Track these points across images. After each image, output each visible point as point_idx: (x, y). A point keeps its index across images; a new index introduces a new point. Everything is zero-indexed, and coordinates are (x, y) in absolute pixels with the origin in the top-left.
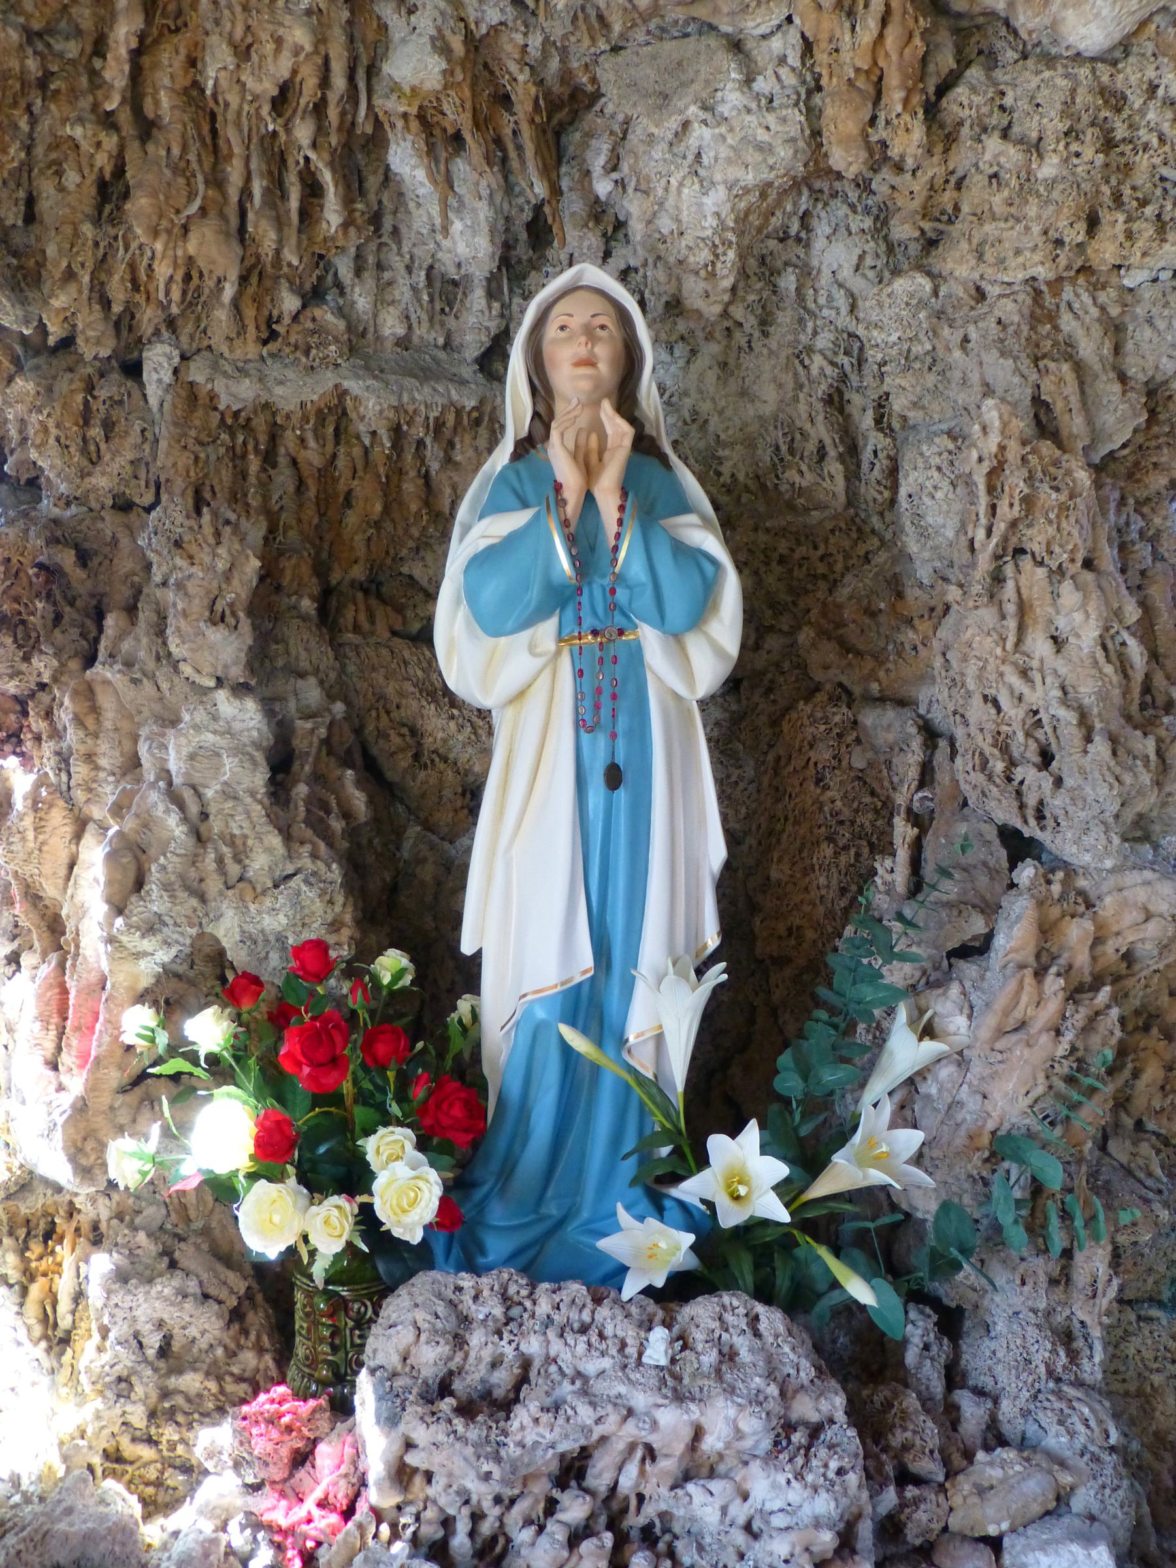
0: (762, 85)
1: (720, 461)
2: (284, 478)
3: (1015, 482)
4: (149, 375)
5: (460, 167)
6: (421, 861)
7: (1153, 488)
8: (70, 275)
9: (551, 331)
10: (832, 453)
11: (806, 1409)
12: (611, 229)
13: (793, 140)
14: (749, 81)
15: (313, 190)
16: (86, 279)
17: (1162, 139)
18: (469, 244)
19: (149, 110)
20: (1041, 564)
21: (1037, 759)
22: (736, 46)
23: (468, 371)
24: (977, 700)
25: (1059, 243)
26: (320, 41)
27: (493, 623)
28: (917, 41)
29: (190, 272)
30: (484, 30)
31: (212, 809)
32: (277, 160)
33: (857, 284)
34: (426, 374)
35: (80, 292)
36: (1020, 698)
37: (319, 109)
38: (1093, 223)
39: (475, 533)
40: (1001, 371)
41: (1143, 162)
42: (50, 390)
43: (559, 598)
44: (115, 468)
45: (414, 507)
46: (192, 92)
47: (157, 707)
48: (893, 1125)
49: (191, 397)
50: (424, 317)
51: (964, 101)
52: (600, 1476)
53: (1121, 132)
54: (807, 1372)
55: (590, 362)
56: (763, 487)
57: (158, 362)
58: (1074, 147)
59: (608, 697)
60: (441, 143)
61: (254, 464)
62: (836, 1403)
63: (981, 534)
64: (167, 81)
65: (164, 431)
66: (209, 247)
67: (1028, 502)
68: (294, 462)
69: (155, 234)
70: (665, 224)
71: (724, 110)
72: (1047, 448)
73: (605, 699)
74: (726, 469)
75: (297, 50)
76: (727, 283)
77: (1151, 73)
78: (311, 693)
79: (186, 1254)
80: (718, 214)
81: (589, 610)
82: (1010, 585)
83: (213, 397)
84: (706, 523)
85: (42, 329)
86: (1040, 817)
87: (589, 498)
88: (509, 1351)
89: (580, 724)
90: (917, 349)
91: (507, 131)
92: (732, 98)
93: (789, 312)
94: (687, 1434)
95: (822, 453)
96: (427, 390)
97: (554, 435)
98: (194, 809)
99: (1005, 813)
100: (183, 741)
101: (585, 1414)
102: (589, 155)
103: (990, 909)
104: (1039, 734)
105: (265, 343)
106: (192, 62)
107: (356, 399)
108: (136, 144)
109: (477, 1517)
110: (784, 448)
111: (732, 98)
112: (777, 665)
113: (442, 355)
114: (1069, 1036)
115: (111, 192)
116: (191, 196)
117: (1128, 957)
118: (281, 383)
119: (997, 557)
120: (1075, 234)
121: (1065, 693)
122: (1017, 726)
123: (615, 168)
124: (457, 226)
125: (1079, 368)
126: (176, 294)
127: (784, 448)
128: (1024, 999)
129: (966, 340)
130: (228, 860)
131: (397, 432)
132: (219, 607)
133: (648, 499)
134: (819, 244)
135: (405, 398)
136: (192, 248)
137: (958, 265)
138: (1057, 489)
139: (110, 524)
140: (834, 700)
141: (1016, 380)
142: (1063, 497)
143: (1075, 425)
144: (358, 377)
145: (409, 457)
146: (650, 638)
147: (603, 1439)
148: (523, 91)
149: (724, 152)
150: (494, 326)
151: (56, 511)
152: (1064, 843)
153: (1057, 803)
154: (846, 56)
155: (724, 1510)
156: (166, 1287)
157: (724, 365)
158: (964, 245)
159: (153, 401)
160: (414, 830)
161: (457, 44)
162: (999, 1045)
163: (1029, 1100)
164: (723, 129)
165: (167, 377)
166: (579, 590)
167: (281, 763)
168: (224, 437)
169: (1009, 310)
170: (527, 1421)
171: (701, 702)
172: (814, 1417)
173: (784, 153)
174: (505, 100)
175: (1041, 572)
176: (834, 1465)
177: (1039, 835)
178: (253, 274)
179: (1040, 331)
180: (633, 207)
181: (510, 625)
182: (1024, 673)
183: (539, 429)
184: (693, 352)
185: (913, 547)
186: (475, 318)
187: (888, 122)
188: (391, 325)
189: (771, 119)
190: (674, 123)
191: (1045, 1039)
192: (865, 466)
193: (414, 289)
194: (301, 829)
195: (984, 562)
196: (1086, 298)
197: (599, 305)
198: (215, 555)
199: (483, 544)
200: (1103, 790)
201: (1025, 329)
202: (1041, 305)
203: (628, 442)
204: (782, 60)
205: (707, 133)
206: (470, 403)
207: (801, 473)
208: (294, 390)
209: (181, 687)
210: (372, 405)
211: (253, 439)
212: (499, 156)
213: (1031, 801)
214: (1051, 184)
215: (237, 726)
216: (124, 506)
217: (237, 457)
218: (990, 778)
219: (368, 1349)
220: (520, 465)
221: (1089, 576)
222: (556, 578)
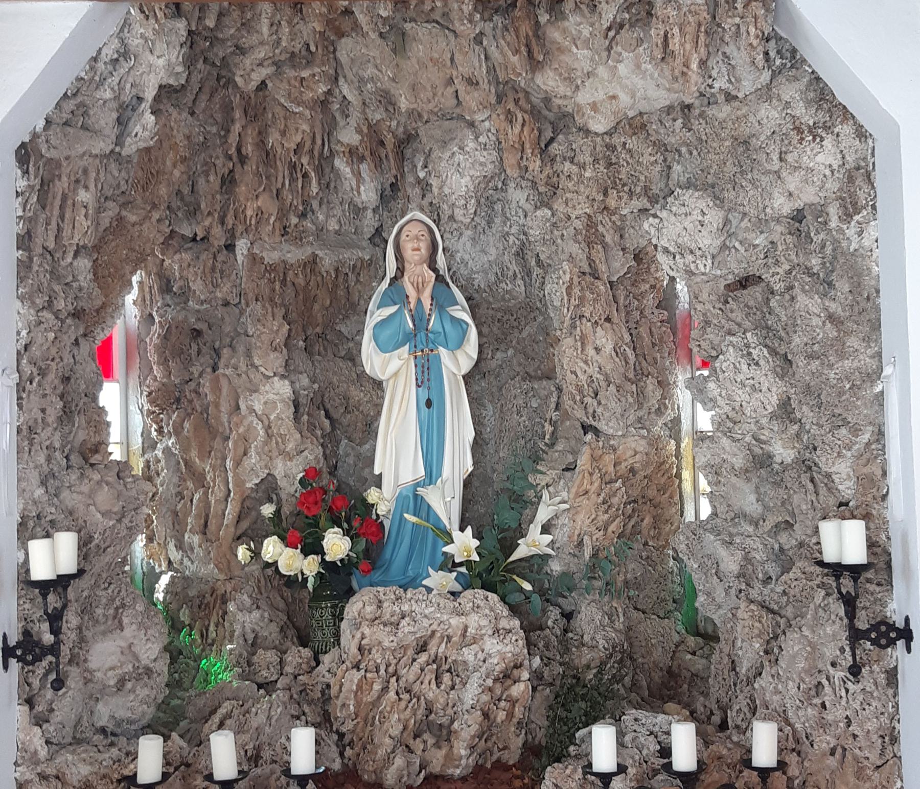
0: (482, 139)
1: (474, 279)
2: (290, 291)
3: (576, 291)
4: (238, 252)
5: (364, 167)
6: (348, 455)
7: (643, 289)
8: (209, 213)
9: (403, 237)
10: (519, 276)
11: (504, 624)
12: (425, 187)
13: (494, 162)
14: (477, 138)
15: (305, 176)
16: (216, 216)
17: (627, 162)
18: (368, 194)
19: (244, 152)
20: (590, 321)
21: (593, 395)
22: (472, 124)
23: (365, 243)
24: (568, 373)
25: (594, 200)
26: (312, 127)
27: (383, 347)
28: (535, 131)
29: (260, 212)
30: (375, 121)
31: (273, 425)
32: (293, 167)
33: (528, 207)
34: (349, 246)
35: (213, 220)
36: (585, 372)
37: (311, 151)
38: (606, 194)
39: (376, 315)
40: (574, 248)
41: (624, 170)
42: (198, 258)
43: (409, 338)
44: (225, 289)
45: (343, 302)
46: (261, 143)
47: (248, 385)
48: (541, 533)
49: (254, 259)
50: (347, 222)
51: (555, 148)
52: (432, 648)
53: (614, 160)
54: (506, 612)
55: (418, 249)
56: (491, 290)
57: (242, 246)
58: (597, 166)
59: (427, 374)
60: (353, 154)
61: (277, 286)
62: (517, 623)
63: (566, 310)
64: (250, 140)
65: (243, 273)
66: (266, 202)
67: (582, 299)
68: (293, 283)
69: (248, 200)
70: (447, 190)
71: (467, 149)
72: (588, 278)
73: (426, 369)
74: (476, 283)
75: (304, 132)
76: (472, 211)
77: (623, 140)
78: (305, 381)
79: (262, 603)
80: (466, 186)
81: (421, 341)
82: (578, 329)
83: (262, 258)
84: (464, 309)
85: (196, 234)
86: (594, 417)
87: (419, 300)
88: (397, 609)
89: (418, 386)
90: (547, 237)
91: (383, 156)
92: (471, 145)
93: (500, 218)
94: (461, 626)
95: (515, 275)
96: (349, 253)
97: (406, 278)
98: (266, 423)
99: (580, 414)
100: (261, 397)
101: (426, 623)
102: (416, 160)
103: (575, 453)
104: (593, 385)
105: (283, 235)
106: (260, 133)
107: (321, 259)
108: (239, 165)
109: (388, 666)
110: (499, 274)
111: (471, 145)
112: (501, 366)
113: (354, 237)
114: (603, 495)
115: (229, 182)
116: (260, 186)
117: (632, 470)
118: (289, 252)
119: (571, 319)
120: (600, 197)
121: (600, 369)
122: (584, 382)
123: (426, 167)
124: (362, 188)
125: (605, 246)
126: (253, 222)
127: (499, 274)
128: (586, 482)
129: (563, 235)
130: (280, 444)
131: (337, 270)
132: (274, 345)
133: (441, 301)
134: (511, 190)
135: (341, 257)
136: (259, 204)
137: (559, 206)
138: (593, 293)
139: (220, 312)
140: (524, 379)
141: (580, 251)
142: (595, 295)
143: (602, 268)
144: (321, 250)
145: (341, 279)
146: (442, 351)
147: (433, 632)
148: (389, 140)
149: (468, 165)
150: (376, 225)
151: (197, 307)
152: (602, 426)
153: (599, 410)
154: (510, 137)
155: (476, 655)
156: (256, 614)
157: (473, 239)
158: (560, 200)
159: (240, 262)
160: (344, 442)
161: (365, 130)
162: (577, 500)
163: (590, 520)
164: (467, 156)
165: (245, 252)
166: (415, 335)
167: (296, 405)
168: (267, 275)
169: (578, 224)
170: (405, 624)
171: (464, 377)
172: (508, 627)
173: (490, 167)
174: (382, 143)
175: (589, 324)
176: (514, 638)
177: (593, 423)
178: (283, 214)
179: (591, 236)
180: (434, 182)
181: (390, 348)
182: (586, 362)
183: (399, 274)
184: (461, 234)
185: (552, 315)
186: (369, 222)
187: (527, 159)
188: (333, 225)
189: (485, 153)
190: (449, 154)
191: (594, 496)
192: (533, 280)
193: (343, 211)
194: (305, 433)
195: (567, 322)
196: (607, 219)
197: (421, 227)
198: (273, 325)
199: (380, 318)
200: (614, 404)
201: (584, 232)
202: (591, 223)
203: (433, 279)
204: (489, 130)
205: (461, 157)
206: (367, 258)
207: (507, 284)
208: (294, 255)
209: (260, 376)
210: (327, 260)
211: (279, 273)
212: (378, 163)
213: (591, 411)
214: (590, 179)
215: (281, 392)
216: (226, 304)
217: (271, 281)
218: (575, 403)
219: (345, 612)
220: (392, 288)
221: (607, 325)
222: (407, 330)
